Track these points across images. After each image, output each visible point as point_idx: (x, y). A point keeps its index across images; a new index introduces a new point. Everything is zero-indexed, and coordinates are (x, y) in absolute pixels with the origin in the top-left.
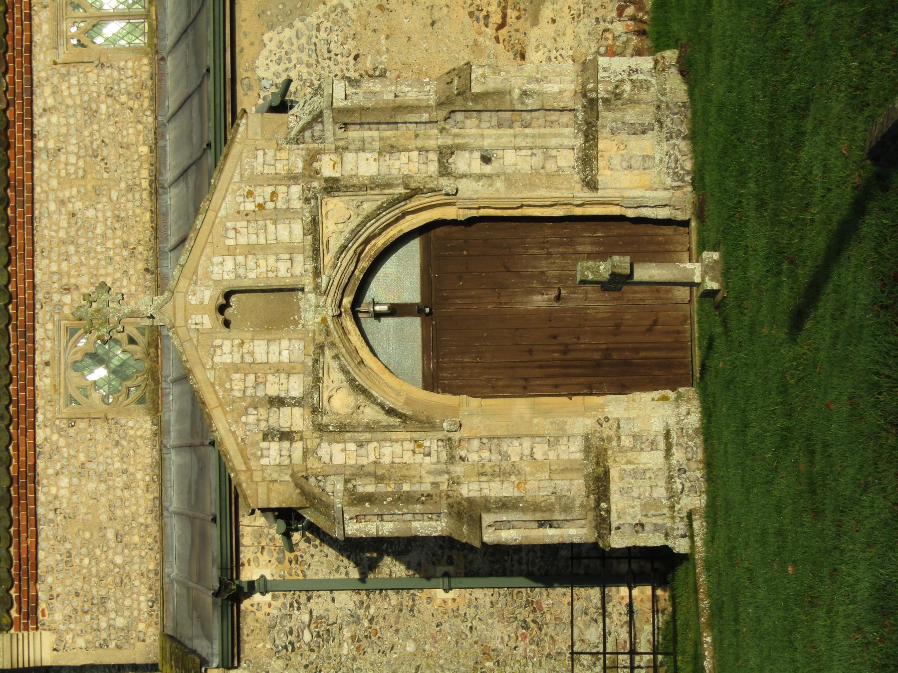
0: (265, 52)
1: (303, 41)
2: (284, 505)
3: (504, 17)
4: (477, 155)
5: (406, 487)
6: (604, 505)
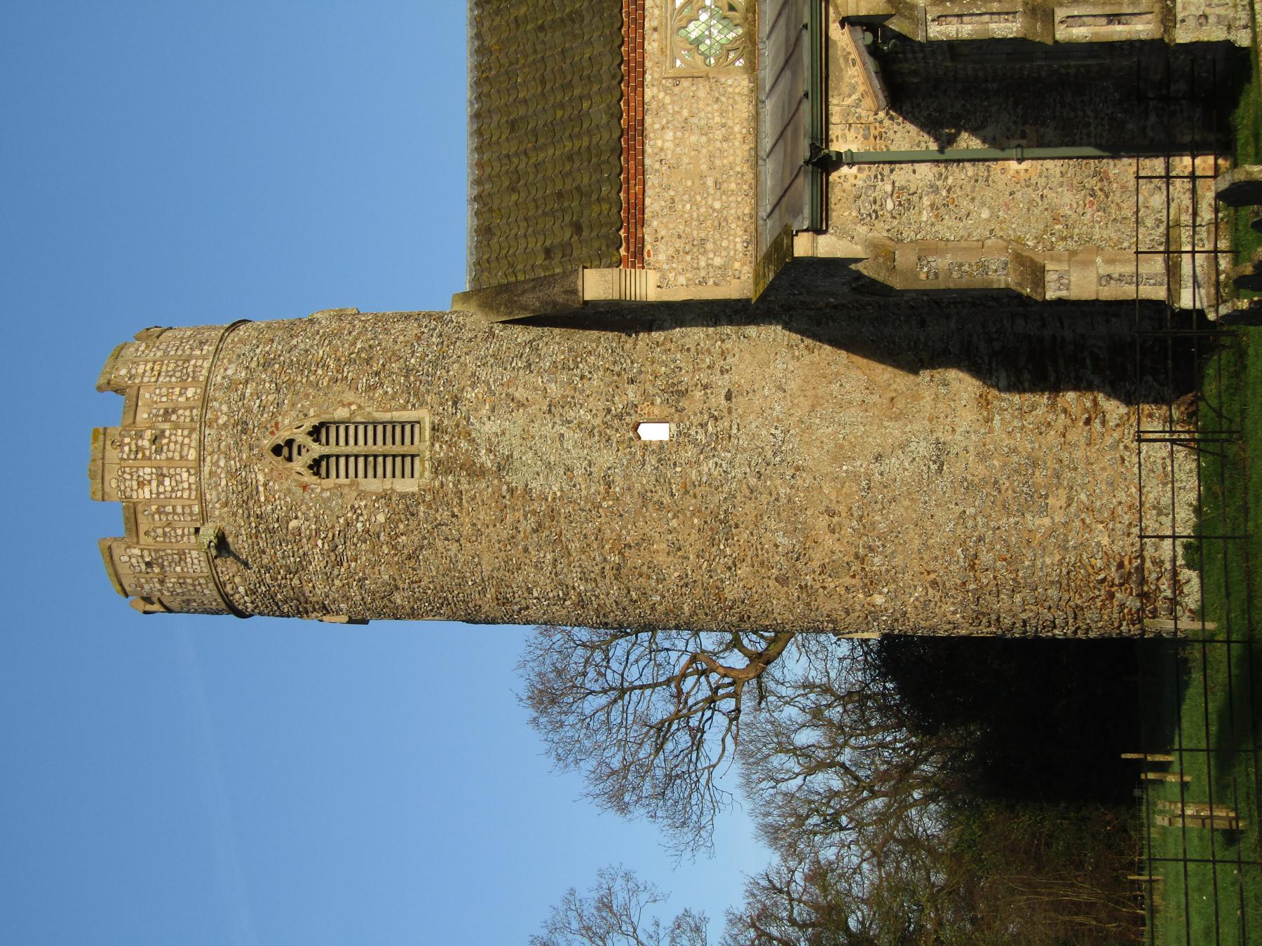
2: (872, 13)
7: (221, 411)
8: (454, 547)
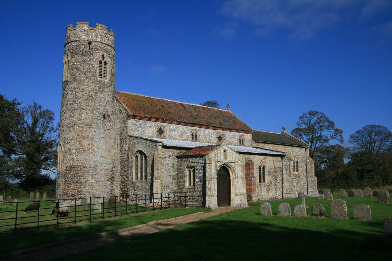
8: (87, 82)
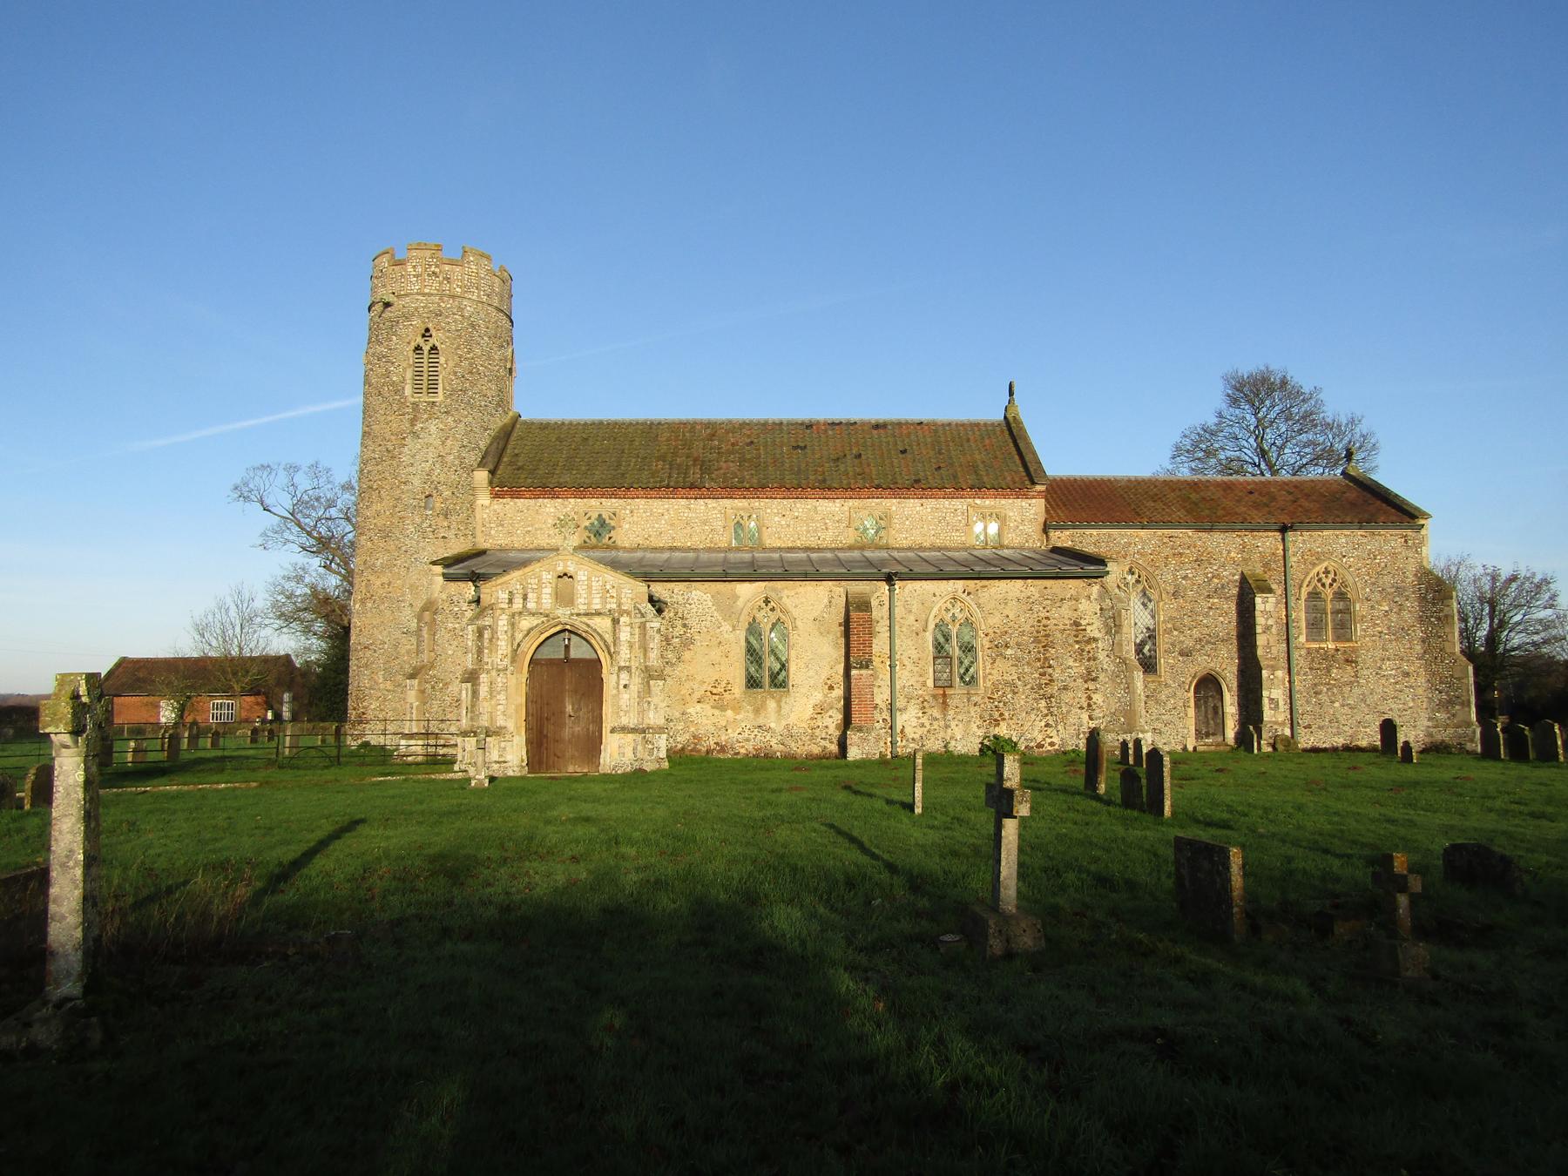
0: (703, 594)
1: (707, 610)
3: (715, 694)
4: (627, 683)
5: (486, 651)
6: (472, 734)
7: (448, 304)
